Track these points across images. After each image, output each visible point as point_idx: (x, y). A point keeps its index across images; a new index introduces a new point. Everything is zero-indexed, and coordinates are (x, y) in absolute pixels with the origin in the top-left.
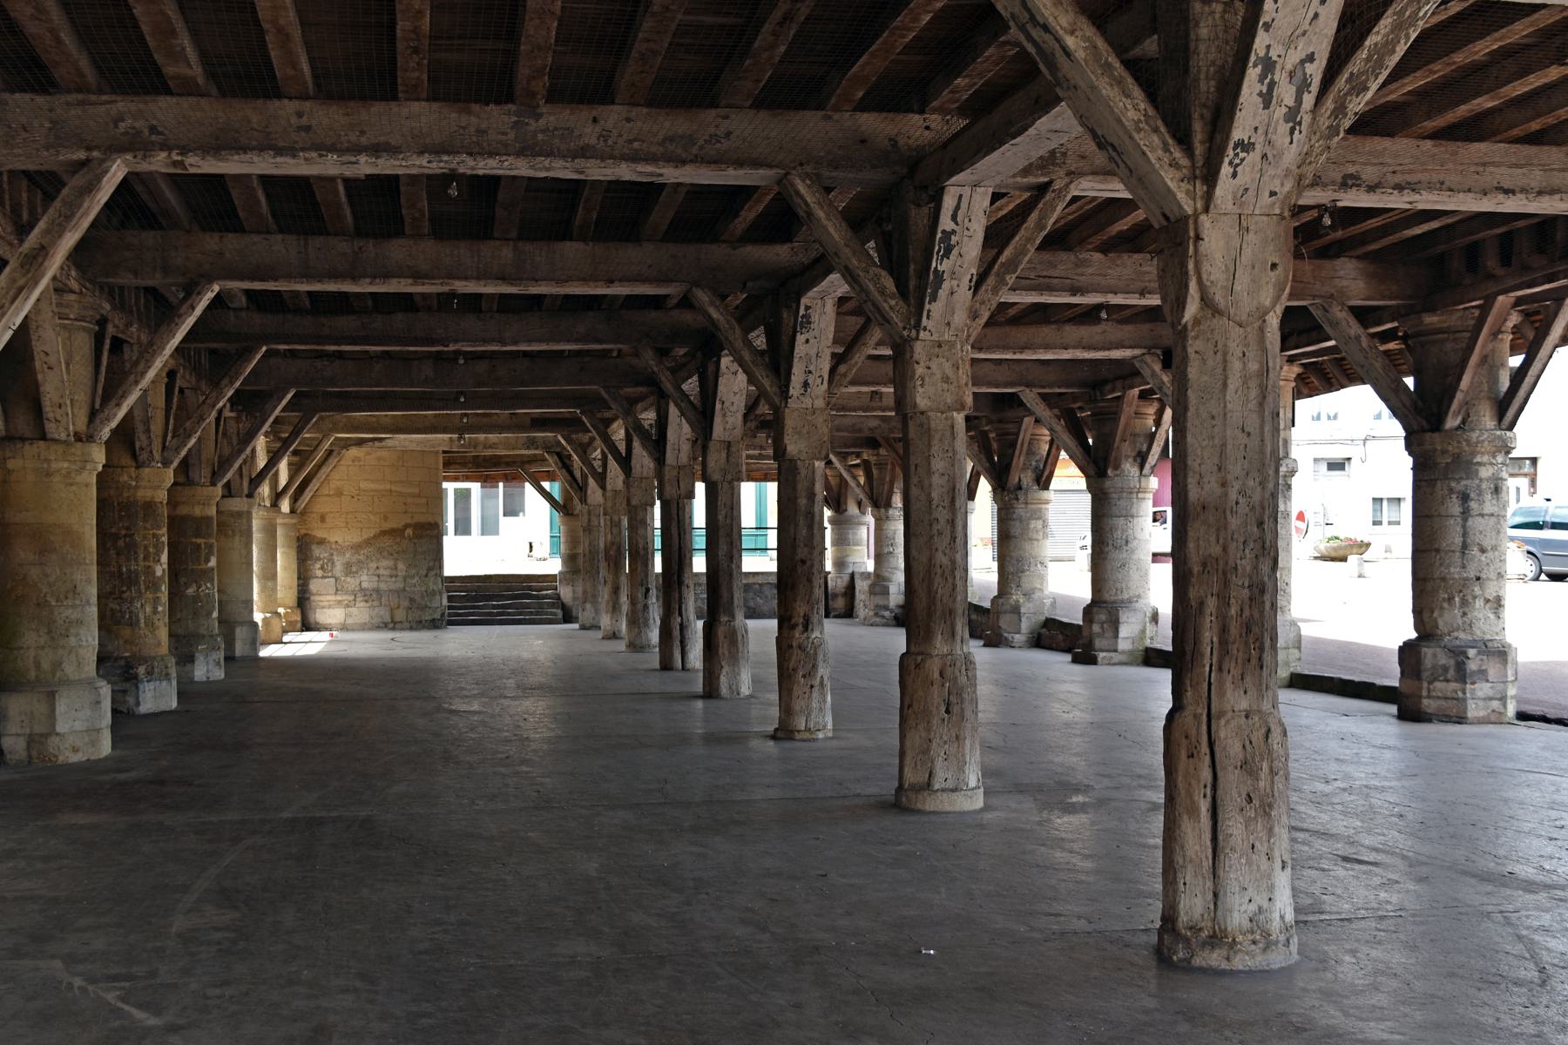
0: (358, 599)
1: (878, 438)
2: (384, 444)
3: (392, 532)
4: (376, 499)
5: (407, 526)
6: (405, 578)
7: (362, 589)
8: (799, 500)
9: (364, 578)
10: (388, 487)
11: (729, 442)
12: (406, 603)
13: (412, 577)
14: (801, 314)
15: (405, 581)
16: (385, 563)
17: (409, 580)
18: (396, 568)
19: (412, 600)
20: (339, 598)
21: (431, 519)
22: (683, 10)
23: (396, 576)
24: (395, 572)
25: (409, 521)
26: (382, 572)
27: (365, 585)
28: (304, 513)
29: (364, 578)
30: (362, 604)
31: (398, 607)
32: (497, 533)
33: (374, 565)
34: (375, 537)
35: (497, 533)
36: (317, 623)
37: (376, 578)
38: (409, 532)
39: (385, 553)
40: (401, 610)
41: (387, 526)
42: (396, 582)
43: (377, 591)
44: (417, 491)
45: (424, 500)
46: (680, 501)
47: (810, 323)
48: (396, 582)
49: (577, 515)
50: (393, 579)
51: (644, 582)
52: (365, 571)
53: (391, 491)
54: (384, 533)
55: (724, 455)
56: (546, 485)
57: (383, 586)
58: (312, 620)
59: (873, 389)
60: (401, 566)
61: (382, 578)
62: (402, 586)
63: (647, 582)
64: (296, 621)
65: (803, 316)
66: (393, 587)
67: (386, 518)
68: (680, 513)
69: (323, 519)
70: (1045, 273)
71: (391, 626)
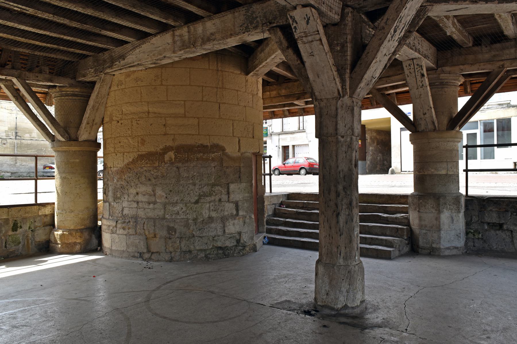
0: (119, 226)
1: (274, 68)
2: (402, 16)
3: (149, 156)
4: (134, 123)
5: (166, 150)
6: (165, 205)
7: (124, 216)
9: (125, 204)
10: (146, 109)
12: (164, 233)
13: (175, 204)
15: (165, 208)
16: (142, 189)
17: (170, 208)
18: (155, 195)
19: (171, 230)
21: (487, 133)
23: (155, 203)
24: (153, 199)
25: (170, 143)
26: (140, 198)
27: (126, 212)
29: (125, 204)
30: (121, 231)
31: (155, 236)
32: (494, 158)
33: (133, 191)
34: (134, 162)
35: (494, 158)
37: (135, 205)
38: (171, 154)
39: (143, 178)
40: (157, 240)
41: (144, 150)
42: (154, 209)
43: (136, 218)
44: (181, 111)
48: (154, 209)
49: (423, 131)
50: (151, 206)
52: (126, 197)
53: (149, 113)
54: (141, 157)
56: (479, 85)
57: (141, 213)
60: (159, 192)
61: (140, 205)
62: (161, 213)
66: (151, 214)
67: (143, 142)
71: (146, 256)
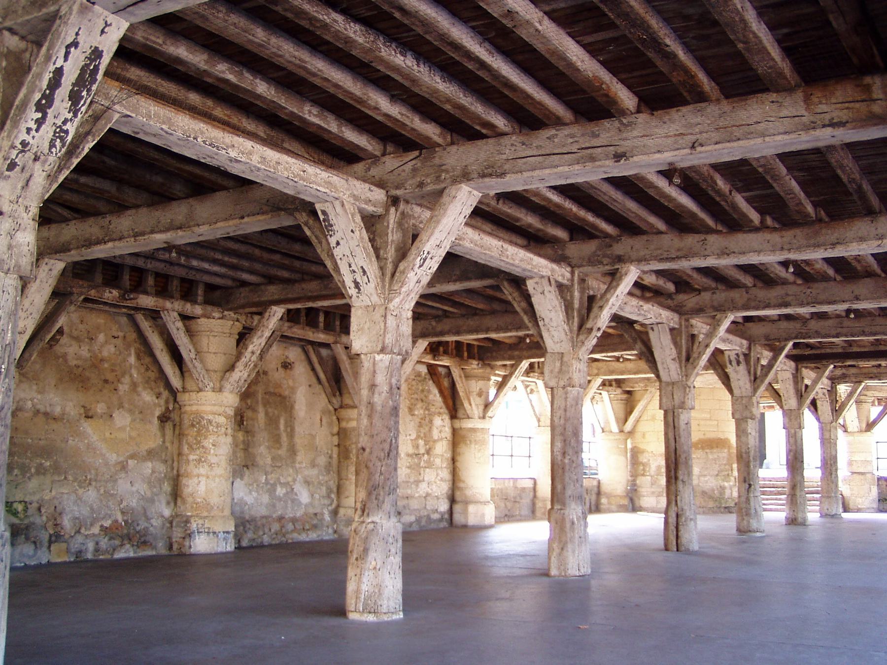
8: (362, 391)
11: (563, 353)
14: (321, 219)
17: (702, 479)
20: (653, 490)
22: (850, 198)
28: (631, 433)
36: (641, 507)
44: (708, 416)
45: (716, 422)
46: (676, 410)
47: (331, 226)
51: (747, 480)
55: (558, 364)
58: (637, 504)
59: (813, 310)
63: (749, 480)
64: (176, 527)
65: (324, 220)
68: (676, 420)
69: (644, 435)
70: (587, 145)
